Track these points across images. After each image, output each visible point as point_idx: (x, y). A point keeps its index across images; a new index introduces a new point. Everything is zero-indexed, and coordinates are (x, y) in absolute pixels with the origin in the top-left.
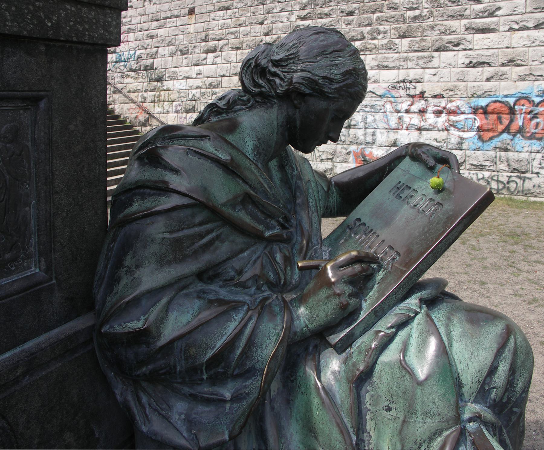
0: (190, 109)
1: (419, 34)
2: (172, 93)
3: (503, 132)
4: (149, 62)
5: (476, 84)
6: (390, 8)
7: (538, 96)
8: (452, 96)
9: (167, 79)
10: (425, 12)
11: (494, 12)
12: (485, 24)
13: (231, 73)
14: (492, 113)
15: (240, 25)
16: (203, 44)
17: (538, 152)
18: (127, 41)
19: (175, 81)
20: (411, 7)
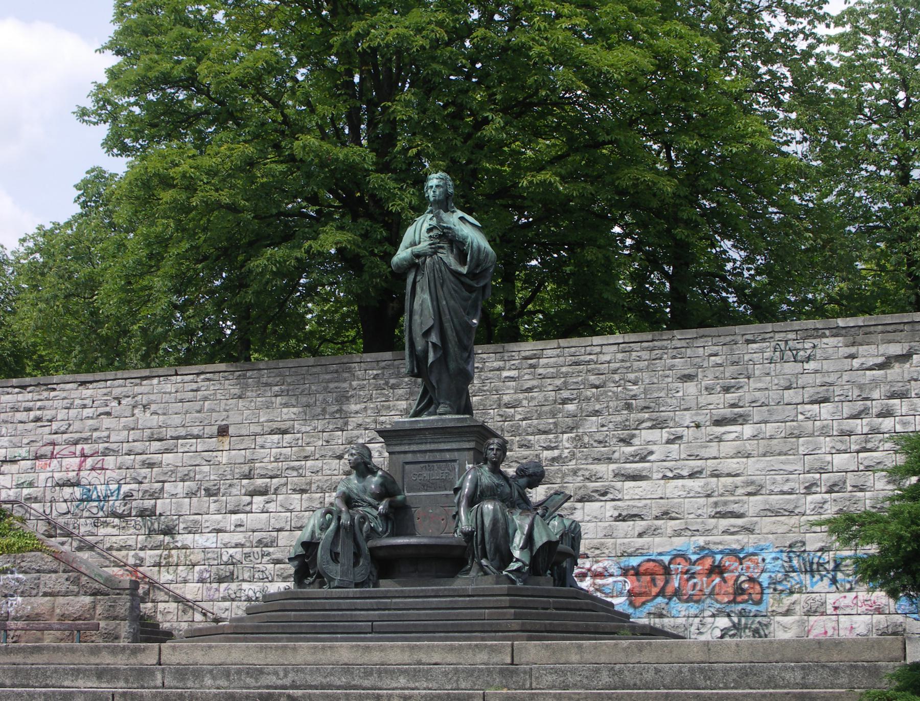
0: (227, 577)
1: (559, 480)
2: (192, 553)
3: (657, 595)
4: (148, 504)
5: (626, 540)
6: (521, 446)
7: (695, 553)
8: (597, 556)
9: (181, 531)
10: (566, 453)
11: (646, 456)
12: (636, 469)
13: (293, 525)
14: (645, 574)
15: (306, 458)
16: (245, 482)
17: (696, 616)
18: (102, 469)
19: (197, 536)
20: (549, 446)
